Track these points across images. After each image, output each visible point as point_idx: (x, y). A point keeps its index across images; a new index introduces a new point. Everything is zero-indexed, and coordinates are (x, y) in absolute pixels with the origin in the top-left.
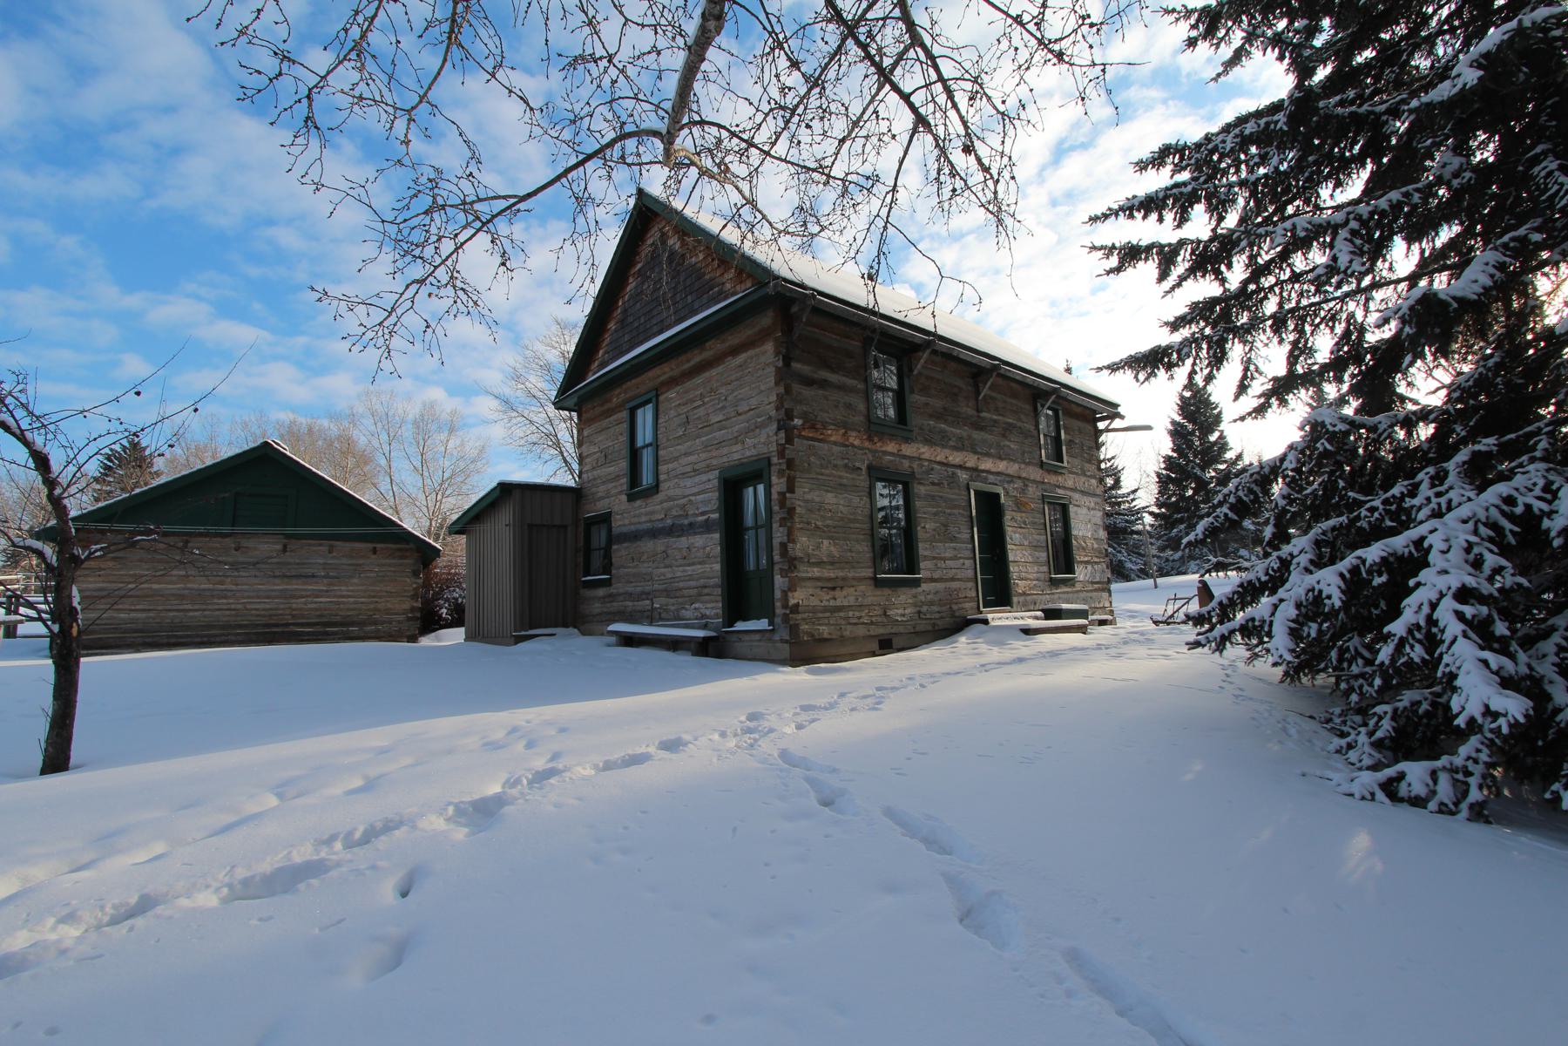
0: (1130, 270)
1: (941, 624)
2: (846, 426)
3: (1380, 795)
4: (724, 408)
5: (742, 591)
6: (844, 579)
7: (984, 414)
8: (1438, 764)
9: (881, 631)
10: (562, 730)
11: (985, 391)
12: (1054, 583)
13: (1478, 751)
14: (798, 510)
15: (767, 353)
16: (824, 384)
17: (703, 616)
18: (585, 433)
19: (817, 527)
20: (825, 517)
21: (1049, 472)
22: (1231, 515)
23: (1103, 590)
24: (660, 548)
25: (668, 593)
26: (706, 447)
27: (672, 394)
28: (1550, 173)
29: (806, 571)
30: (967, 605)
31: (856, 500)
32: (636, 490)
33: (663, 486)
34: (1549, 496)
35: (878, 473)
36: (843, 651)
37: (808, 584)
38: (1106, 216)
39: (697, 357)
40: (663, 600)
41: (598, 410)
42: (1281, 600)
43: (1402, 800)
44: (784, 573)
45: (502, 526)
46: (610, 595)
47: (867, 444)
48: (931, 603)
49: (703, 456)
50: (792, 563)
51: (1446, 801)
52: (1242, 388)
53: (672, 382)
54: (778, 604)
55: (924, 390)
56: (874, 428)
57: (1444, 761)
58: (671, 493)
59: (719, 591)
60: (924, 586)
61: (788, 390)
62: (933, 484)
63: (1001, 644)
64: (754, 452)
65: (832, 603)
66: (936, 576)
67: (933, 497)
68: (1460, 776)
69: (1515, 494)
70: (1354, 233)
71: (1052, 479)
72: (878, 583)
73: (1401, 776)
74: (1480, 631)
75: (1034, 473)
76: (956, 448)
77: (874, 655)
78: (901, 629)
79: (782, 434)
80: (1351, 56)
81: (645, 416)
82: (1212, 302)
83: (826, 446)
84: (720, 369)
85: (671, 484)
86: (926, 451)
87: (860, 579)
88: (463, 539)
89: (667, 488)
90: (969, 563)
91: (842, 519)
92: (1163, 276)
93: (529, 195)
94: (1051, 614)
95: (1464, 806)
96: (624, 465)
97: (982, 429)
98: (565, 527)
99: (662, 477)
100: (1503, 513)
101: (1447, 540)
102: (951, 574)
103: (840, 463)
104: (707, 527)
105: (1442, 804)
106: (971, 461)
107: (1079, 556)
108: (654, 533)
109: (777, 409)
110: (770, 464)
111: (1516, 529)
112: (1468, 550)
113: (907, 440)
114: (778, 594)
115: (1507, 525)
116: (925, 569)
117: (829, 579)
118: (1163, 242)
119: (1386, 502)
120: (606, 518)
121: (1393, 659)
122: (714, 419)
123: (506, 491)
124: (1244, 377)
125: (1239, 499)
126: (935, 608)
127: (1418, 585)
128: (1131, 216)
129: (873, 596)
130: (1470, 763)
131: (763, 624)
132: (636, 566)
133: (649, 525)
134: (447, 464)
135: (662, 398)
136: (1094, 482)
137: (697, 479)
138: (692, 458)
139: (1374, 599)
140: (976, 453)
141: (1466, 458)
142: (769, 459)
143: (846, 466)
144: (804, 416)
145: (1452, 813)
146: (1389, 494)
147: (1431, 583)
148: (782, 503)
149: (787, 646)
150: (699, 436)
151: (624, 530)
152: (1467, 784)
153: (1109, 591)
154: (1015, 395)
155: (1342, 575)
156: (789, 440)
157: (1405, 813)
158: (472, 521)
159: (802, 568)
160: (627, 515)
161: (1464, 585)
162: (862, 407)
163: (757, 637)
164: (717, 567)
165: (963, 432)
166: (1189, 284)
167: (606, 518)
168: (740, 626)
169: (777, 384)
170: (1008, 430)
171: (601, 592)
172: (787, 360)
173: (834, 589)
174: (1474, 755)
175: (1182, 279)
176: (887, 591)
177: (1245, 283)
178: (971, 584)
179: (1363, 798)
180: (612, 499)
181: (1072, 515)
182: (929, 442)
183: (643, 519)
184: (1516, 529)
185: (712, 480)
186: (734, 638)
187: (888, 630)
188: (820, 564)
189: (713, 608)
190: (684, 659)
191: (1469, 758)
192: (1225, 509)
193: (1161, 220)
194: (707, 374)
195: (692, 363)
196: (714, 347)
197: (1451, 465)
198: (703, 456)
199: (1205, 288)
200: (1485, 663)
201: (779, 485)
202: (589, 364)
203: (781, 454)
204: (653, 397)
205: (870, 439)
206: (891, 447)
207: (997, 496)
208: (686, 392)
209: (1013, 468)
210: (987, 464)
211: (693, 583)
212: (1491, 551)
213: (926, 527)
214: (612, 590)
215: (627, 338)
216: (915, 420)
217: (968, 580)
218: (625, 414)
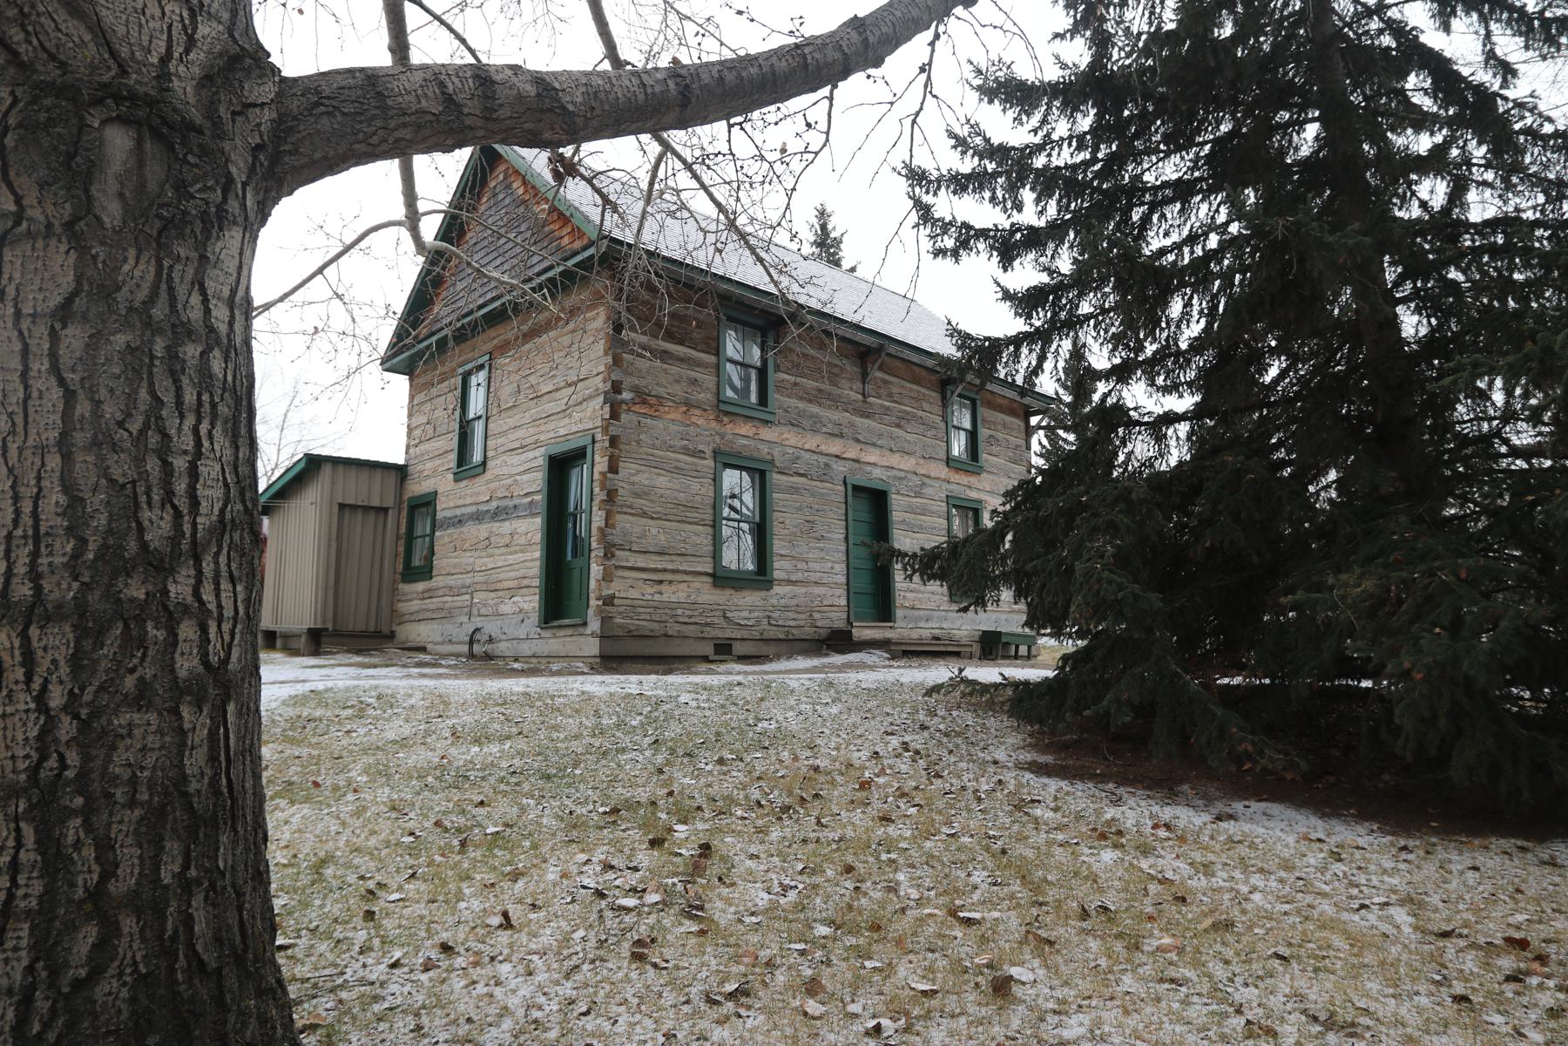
2: (689, 405)
14: (621, 491)
21: (958, 470)
32: (465, 466)
33: (490, 464)
35: (727, 459)
48: (786, 608)
49: (532, 431)
56: (723, 409)
58: (498, 471)
60: (777, 589)
61: (617, 361)
65: (657, 597)
75: (941, 471)
79: (607, 408)
85: (498, 461)
86: (791, 438)
99: (490, 454)
102: (814, 577)
108: (478, 517)
109: (605, 381)
120: (426, 503)
133: (473, 509)
138: (520, 433)
144: (636, 390)
151: (449, 514)
154: (916, 381)
160: (453, 496)
167: (426, 503)
169: (606, 354)
180: (435, 477)
198: (532, 431)
203: (605, 429)
205: (718, 420)
206: (746, 429)
210: (872, 456)
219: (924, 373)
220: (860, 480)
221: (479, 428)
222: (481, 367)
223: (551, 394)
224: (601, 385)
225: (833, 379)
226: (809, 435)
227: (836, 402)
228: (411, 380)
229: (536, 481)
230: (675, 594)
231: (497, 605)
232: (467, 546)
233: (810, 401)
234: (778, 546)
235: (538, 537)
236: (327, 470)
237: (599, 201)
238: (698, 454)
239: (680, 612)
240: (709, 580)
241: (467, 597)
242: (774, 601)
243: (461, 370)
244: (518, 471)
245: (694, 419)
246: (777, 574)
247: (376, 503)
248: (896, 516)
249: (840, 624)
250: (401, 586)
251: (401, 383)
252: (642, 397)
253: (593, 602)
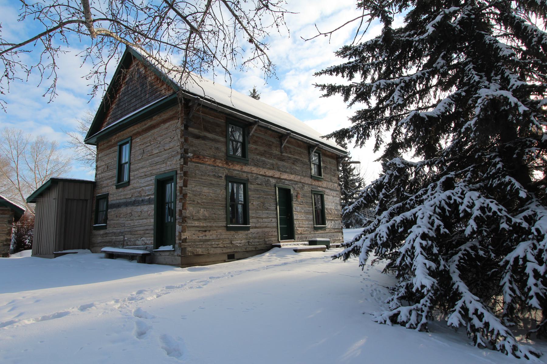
0: (332, 96)
1: (259, 247)
2: (215, 158)
3: (388, 322)
4: (159, 147)
5: (163, 233)
6: (211, 227)
7: (284, 154)
8: (412, 307)
9: (229, 250)
10: (37, 301)
11: (285, 144)
12: (316, 229)
13: (427, 301)
14: (189, 195)
15: (177, 125)
16: (204, 138)
17: (146, 244)
18: (100, 156)
19: (198, 203)
20: (201, 199)
21: (315, 180)
22: (364, 201)
23: (339, 232)
24: (129, 211)
25: (131, 233)
26: (151, 165)
27: (138, 140)
28: (470, 69)
29: (190, 223)
30: (273, 239)
31: (218, 191)
32: (121, 183)
33: (132, 182)
34: (463, 196)
36: (208, 260)
37: (191, 229)
38: (321, 73)
39: (149, 123)
40: (129, 236)
41: (106, 145)
42: (367, 238)
43: (398, 323)
44: (180, 224)
45: (52, 201)
46: (106, 233)
47: (225, 166)
48: (255, 238)
50: (184, 219)
51: (413, 323)
52: (377, 147)
53: (138, 134)
54: (177, 238)
55: (255, 142)
56: (229, 159)
57: (414, 306)
58: (135, 185)
59: (152, 232)
60: (251, 230)
61: (186, 140)
62: (258, 184)
63: (282, 256)
64: (170, 168)
65: (204, 238)
66: (258, 225)
67: (257, 190)
68: (420, 312)
69: (452, 195)
70: (402, 88)
71: (317, 183)
72: (228, 229)
73: (399, 313)
74: (427, 250)
75: (308, 181)
76: (270, 169)
77: (225, 261)
78: (239, 250)
79: (182, 160)
80: (419, 16)
81: (126, 149)
82: (366, 111)
83: (204, 166)
84: (158, 129)
85: (135, 181)
86: (255, 170)
87: (219, 227)
88: (34, 205)
89: (134, 183)
90: (274, 220)
91: (211, 199)
92: (346, 99)
93: (21, 45)
94: (312, 243)
95: (419, 325)
96: (115, 172)
97: (283, 160)
98: (87, 200)
99: (131, 178)
100: (446, 203)
101: (423, 214)
102: (265, 225)
103: (211, 174)
104: (149, 202)
105: (412, 324)
106: (277, 174)
107: (328, 217)
108: (126, 204)
110: (176, 174)
111: (450, 209)
112: (430, 218)
113: (246, 164)
114: (177, 234)
115: (446, 207)
116: (252, 222)
117: (203, 227)
118: (345, 85)
119: (416, 197)
120: (106, 197)
121: (401, 263)
122: (155, 152)
123: (54, 183)
124: (377, 143)
125: (368, 195)
126: (257, 240)
127: (411, 232)
128: (331, 74)
130: (423, 307)
131: (170, 248)
132: (118, 220)
133: (125, 200)
134: (49, 167)
135: (133, 141)
136: (336, 185)
137: (146, 179)
138: (145, 170)
139: (396, 236)
140: (279, 171)
141: (443, 180)
142: (176, 171)
143: (214, 175)
144: (194, 152)
145: (415, 328)
146: (417, 194)
147: (416, 231)
148: (181, 192)
149: (180, 258)
150: (148, 160)
151: (114, 202)
152: (422, 315)
153: (342, 233)
154: (299, 146)
155: (388, 228)
156: (185, 163)
157: (398, 327)
158: (37, 197)
159: (189, 221)
160: (117, 196)
161: (424, 232)
162: (224, 149)
163: (168, 253)
164: (152, 220)
165: (274, 161)
166: (357, 103)
167: (106, 197)
168: (162, 248)
169: (181, 137)
170: (295, 162)
171: (102, 232)
172: (186, 127)
173: (205, 231)
174: (425, 303)
175: (354, 101)
176: (233, 232)
177: (378, 104)
178: (275, 229)
179: (381, 323)
180: (109, 188)
181: (325, 199)
182: (256, 165)
183: (122, 197)
184: (450, 209)
185: (152, 180)
186: (158, 254)
187: (233, 250)
188: (199, 220)
189: (150, 240)
190: (134, 264)
191: (423, 304)
192: (362, 199)
193: (343, 76)
194: (153, 131)
195: (147, 126)
196: (157, 119)
197: (438, 183)
199: (362, 106)
200: (425, 264)
201: (180, 183)
202: (103, 124)
203: (182, 169)
204: (130, 141)
205: (227, 163)
206: (238, 167)
207: (289, 190)
208: (144, 139)
209: (297, 178)
210: (285, 176)
211: (142, 228)
212: (437, 218)
213: (253, 204)
214: (107, 231)
215: (119, 112)
216: (251, 156)
217: (273, 227)
218: (117, 148)
219: (302, 143)
221: (127, 166)
222: (127, 143)
223: (159, 150)
224: (179, 150)
225: (270, 146)
226: (261, 169)
227: (271, 156)
228: (97, 148)
231: (135, 241)
232: (122, 215)
233: (262, 155)
235: (153, 213)
236: (61, 184)
237: (188, 28)
239: (213, 243)
240: (224, 228)
241: (122, 237)
242: (250, 235)
243: (119, 144)
244: (144, 185)
245: (217, 164)
247: (82, 197)
251: (94, 148)
252: (197, 156)
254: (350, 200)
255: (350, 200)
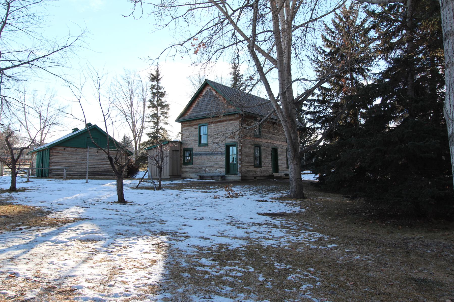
2: (250, 136)
25: (210, 167)
27: (212, 125)
48: (263, 171)
60: (262, 168)
84: (226, 123)
96: (198, 138)
102: (267, 165)
104: (222, 154)
108: (206, 154)
114: (238, 168)
129: (254, 169)
160: (196, 149)
206: (258, 140)
218: (198, 127)
220: (273, 147)
229: (223, 149)
230: (249, 169)
234: (262, 160)
238: (251, 145)
246: (262, 165)
248: (279, 153)
249: (271, 174)
250: (182, 166)
251: (180, 124)
253: (239, 171)
254: (404, 32)
255: (404, 32)
